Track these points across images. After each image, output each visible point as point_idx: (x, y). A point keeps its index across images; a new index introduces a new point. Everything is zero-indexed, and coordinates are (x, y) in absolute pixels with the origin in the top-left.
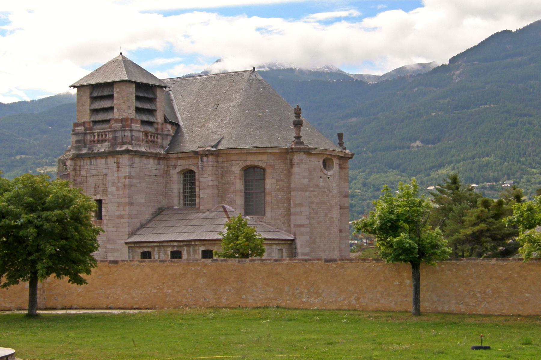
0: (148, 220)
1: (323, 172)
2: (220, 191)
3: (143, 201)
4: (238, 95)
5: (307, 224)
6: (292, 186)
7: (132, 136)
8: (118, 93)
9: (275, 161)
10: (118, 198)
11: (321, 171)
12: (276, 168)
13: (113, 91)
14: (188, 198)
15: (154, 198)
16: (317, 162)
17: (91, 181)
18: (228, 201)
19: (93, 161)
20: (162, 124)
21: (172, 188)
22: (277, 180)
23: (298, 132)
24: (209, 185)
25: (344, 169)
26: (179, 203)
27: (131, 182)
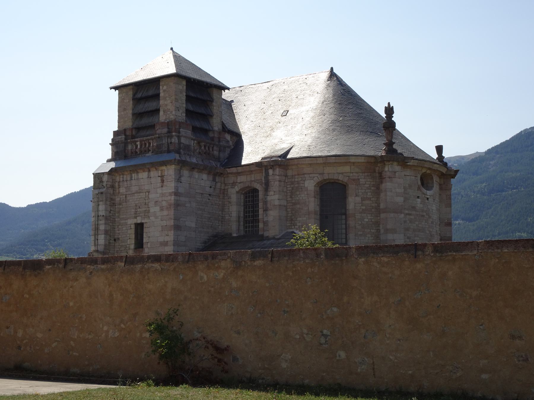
2: (289, 213)
3: (193, 225)
4: (312, 99)
6: (382, 206)
7: (180, 143)
8: (164, 91)
11: (419, 189)
12: (361, 183)
13: (159, 89)
14: (249, 224)
16: (414, 177)
17: (131, 200)
18: (299, 226)
19: (134, 176)
20: (220, 133)
21: (230, 211)
22: (363, 199)
23: (389, 138)
24: (275, 205)
26: (239, 230)
27: (177, 200)
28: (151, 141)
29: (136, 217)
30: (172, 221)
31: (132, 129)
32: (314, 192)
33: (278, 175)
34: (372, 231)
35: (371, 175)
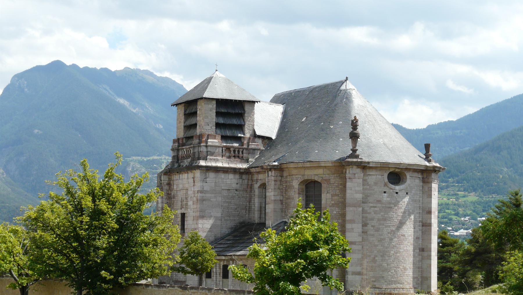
0: (226, 234)
1: (388, 187)
5: (360, 242)
7: (207, 152)
9: (331, 175)
10: (193, 212)
11: (385, 185)
12: (331, 182)
15: (234, 212)
22: (333, 196)
25: (428, 183)
28: (191, 149)
29: (181, 209)
30: (199, 213)
31: (183, 139)
32: (299, 190)
33: (273, 176)
34: (339, 221)
35: (339, 176)
